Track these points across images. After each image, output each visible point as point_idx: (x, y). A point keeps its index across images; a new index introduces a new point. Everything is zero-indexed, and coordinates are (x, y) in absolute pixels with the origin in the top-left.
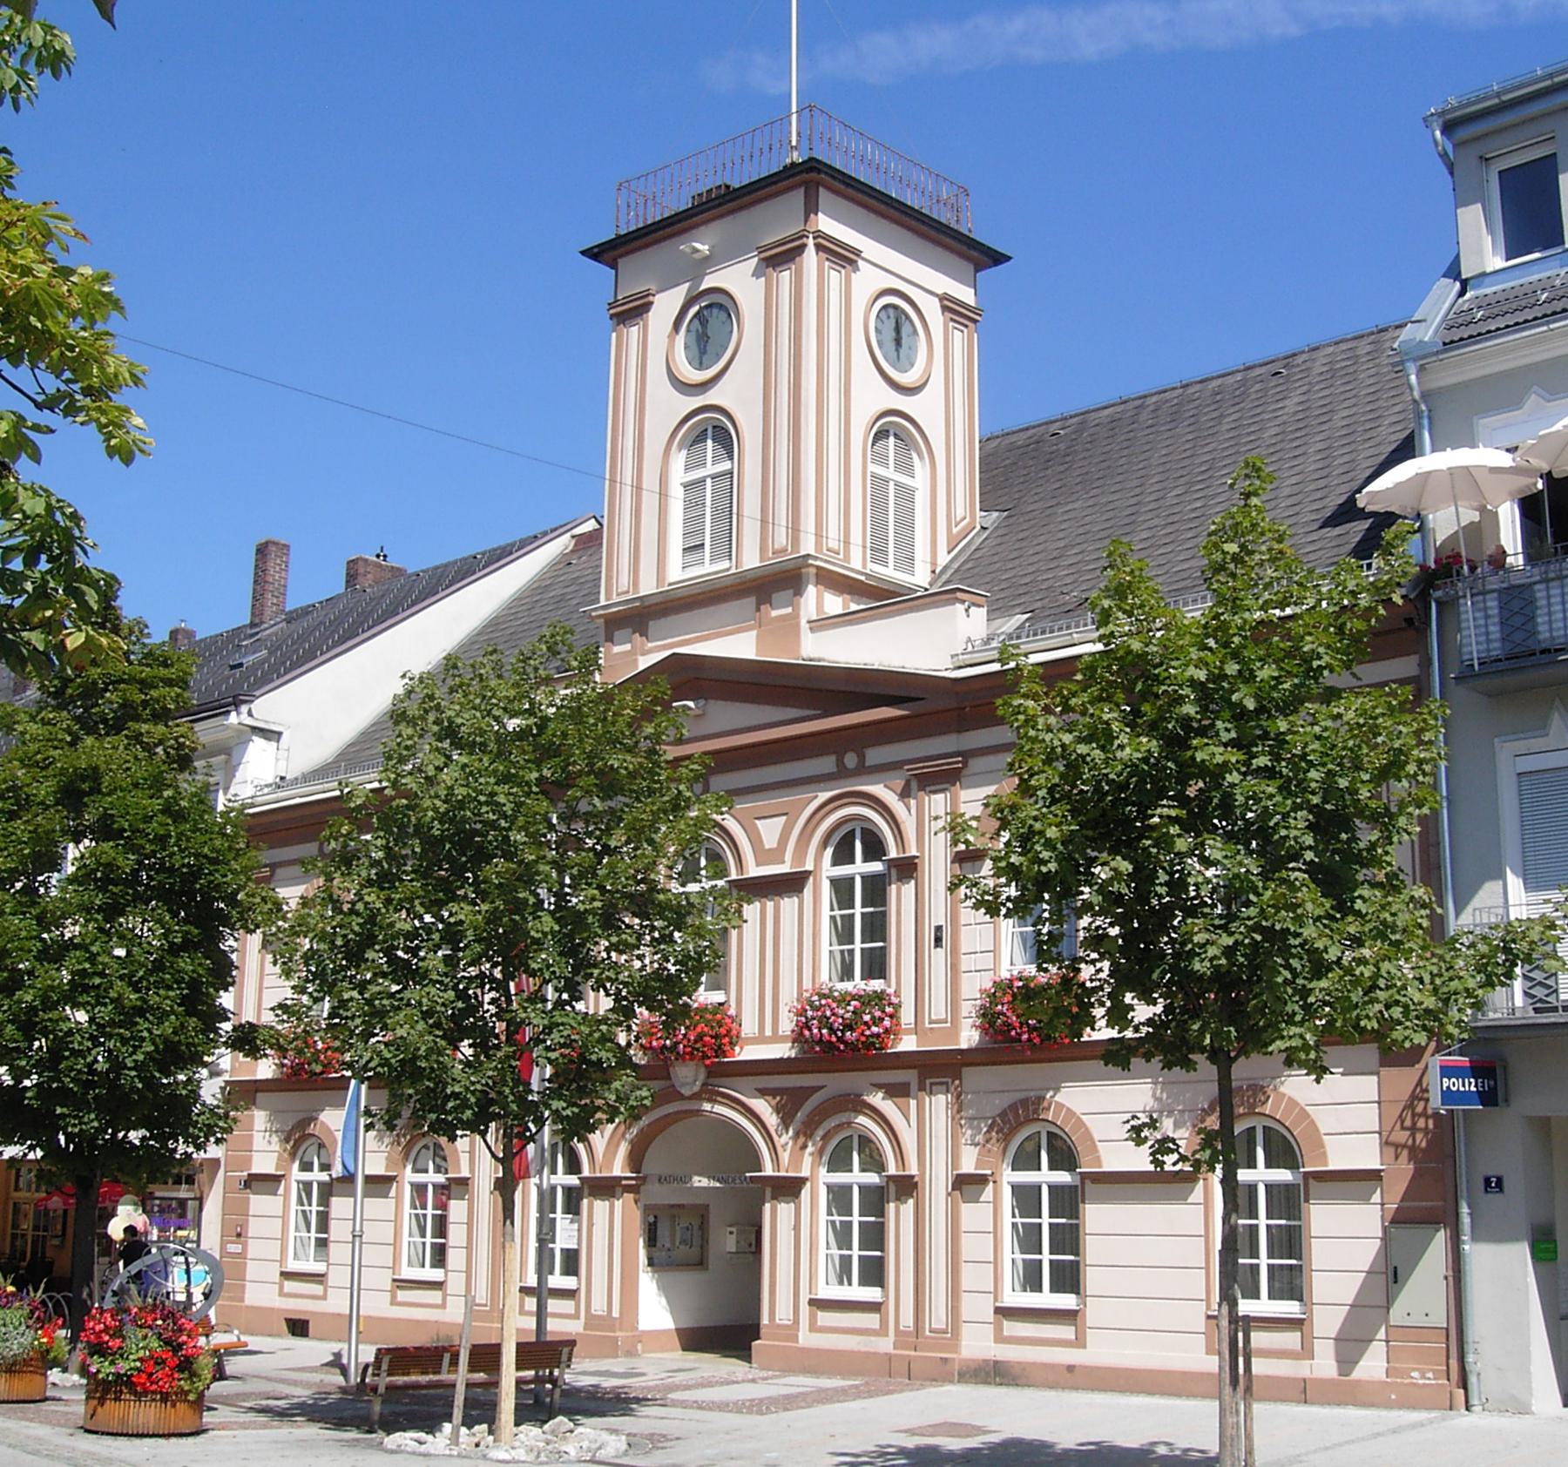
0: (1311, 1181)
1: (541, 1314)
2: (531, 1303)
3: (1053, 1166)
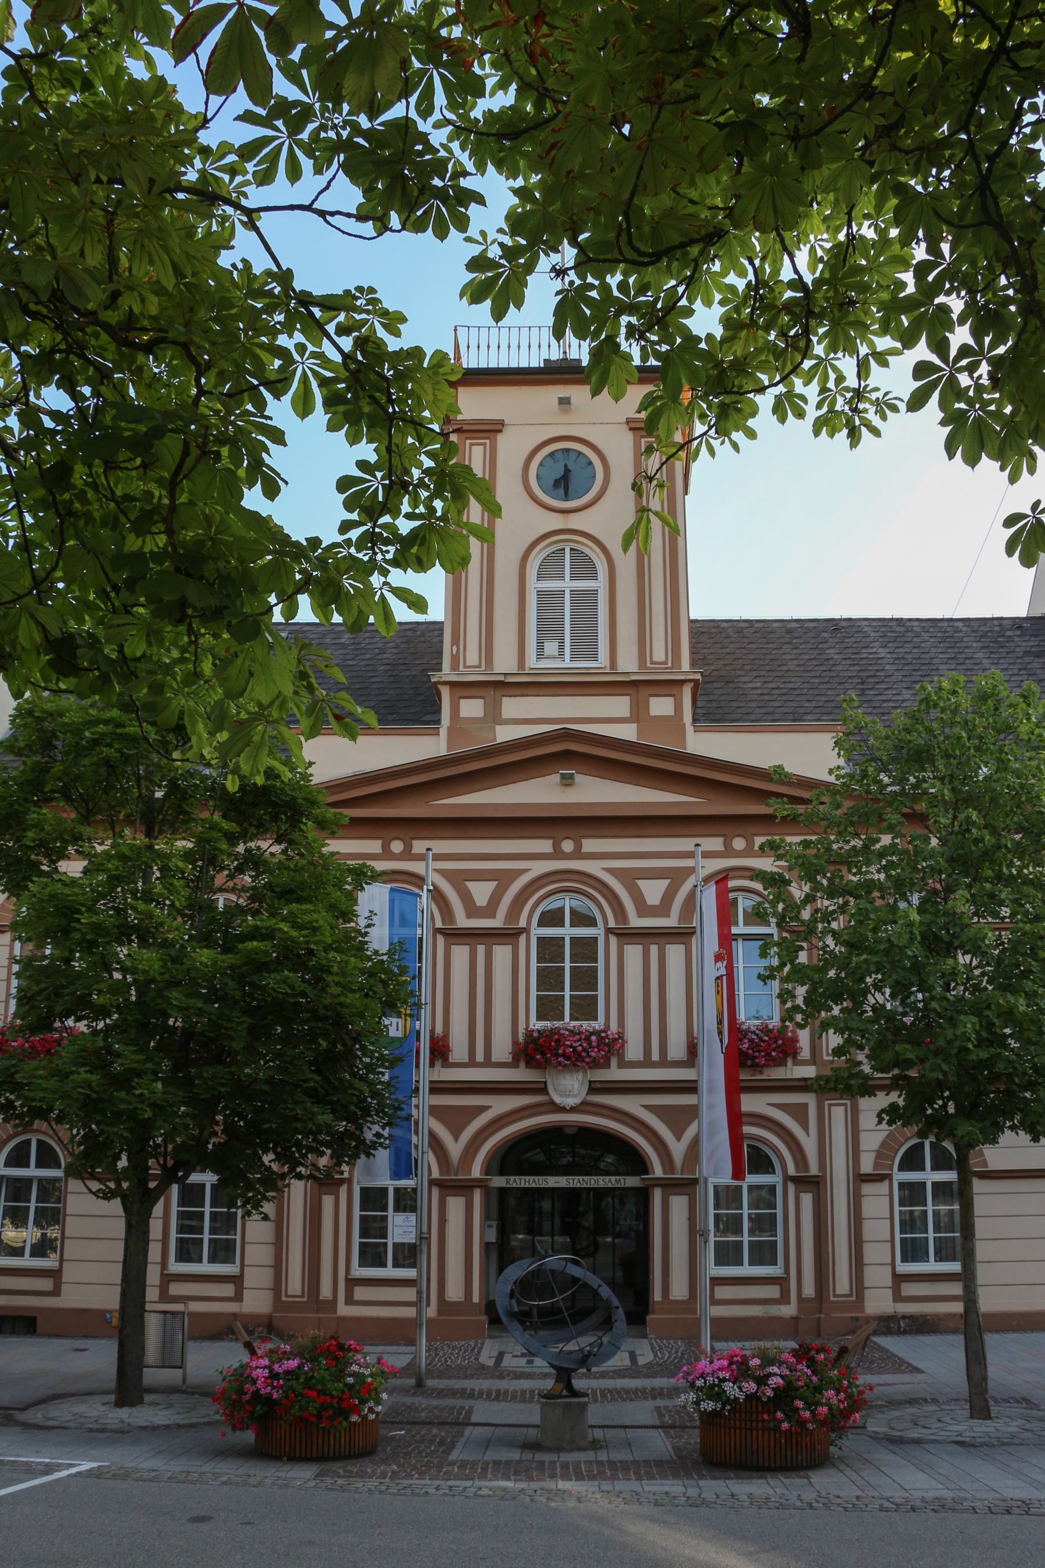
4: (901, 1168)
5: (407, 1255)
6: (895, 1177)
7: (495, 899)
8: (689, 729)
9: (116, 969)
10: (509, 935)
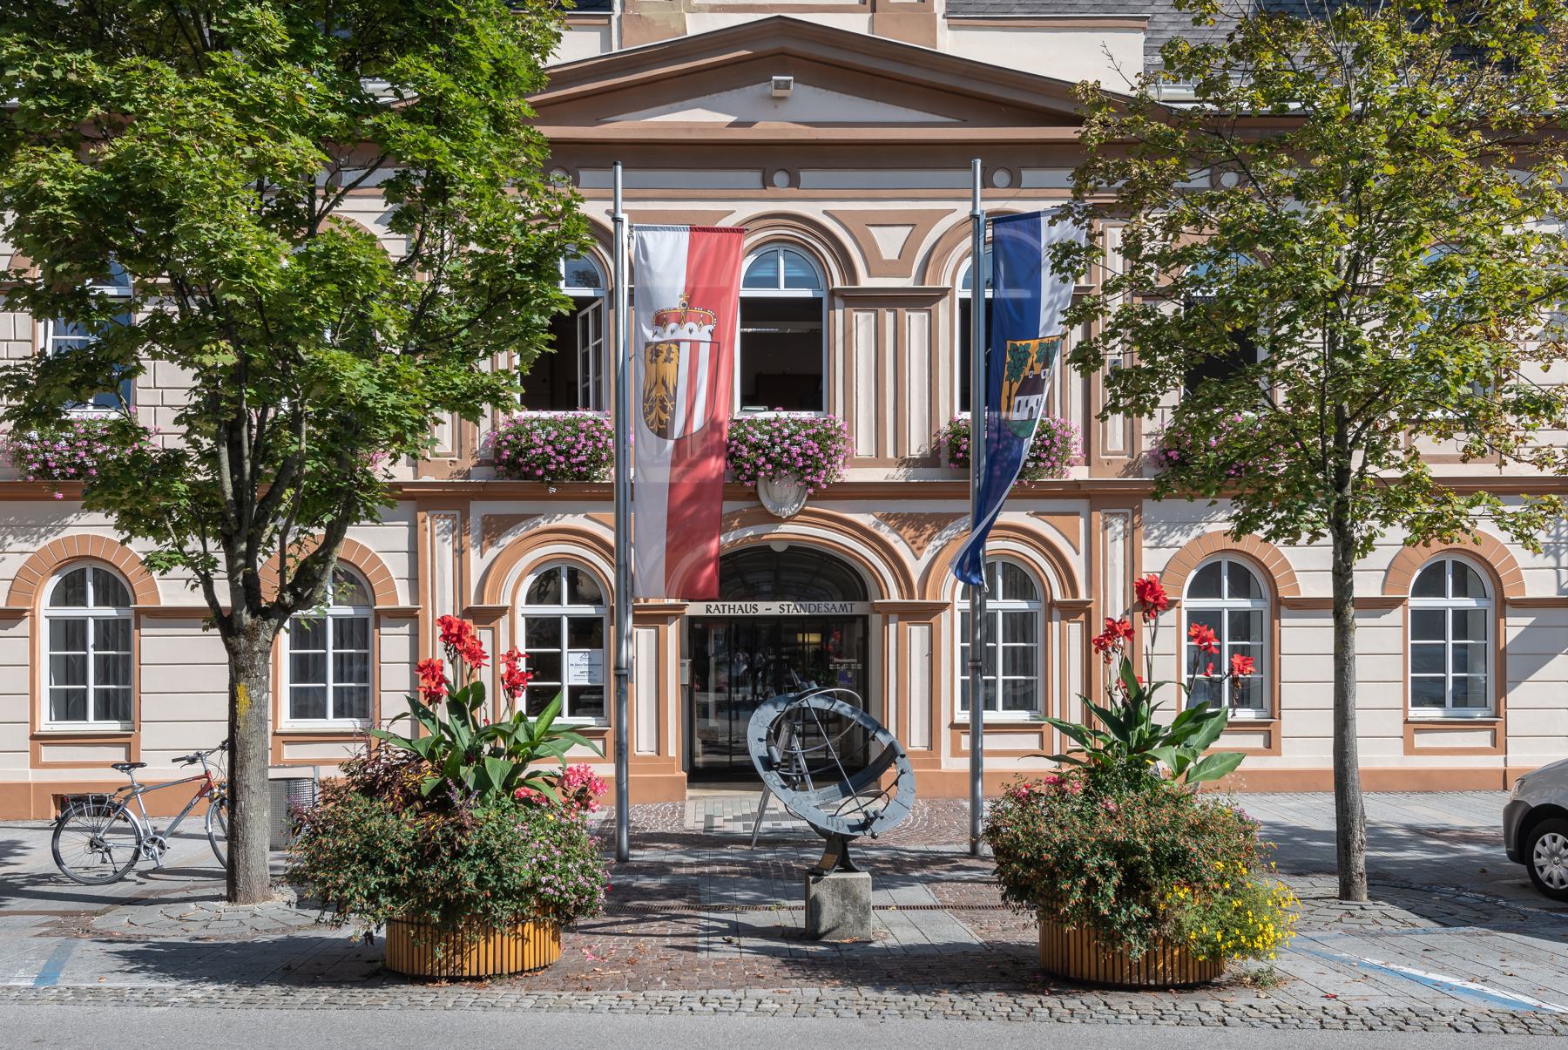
0: (143, 617)
1: (976, 756)
2: (966, 742)
3: (101, 600)
4: (1192, 594)
5: (585, 700)
6: (1184, 605)
7: (907, 250)
8: (941, 22)
9: (1087, 332)
10: (923, 299)
